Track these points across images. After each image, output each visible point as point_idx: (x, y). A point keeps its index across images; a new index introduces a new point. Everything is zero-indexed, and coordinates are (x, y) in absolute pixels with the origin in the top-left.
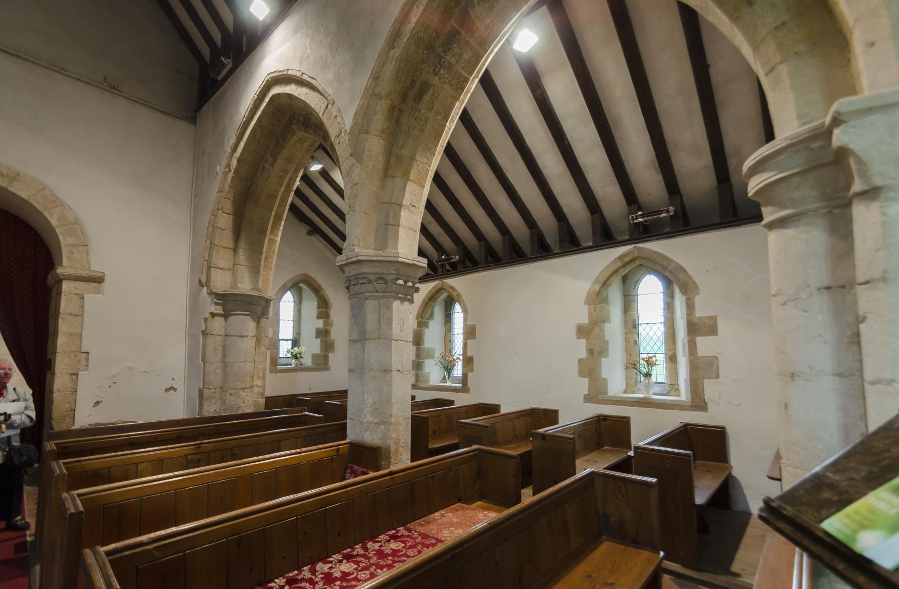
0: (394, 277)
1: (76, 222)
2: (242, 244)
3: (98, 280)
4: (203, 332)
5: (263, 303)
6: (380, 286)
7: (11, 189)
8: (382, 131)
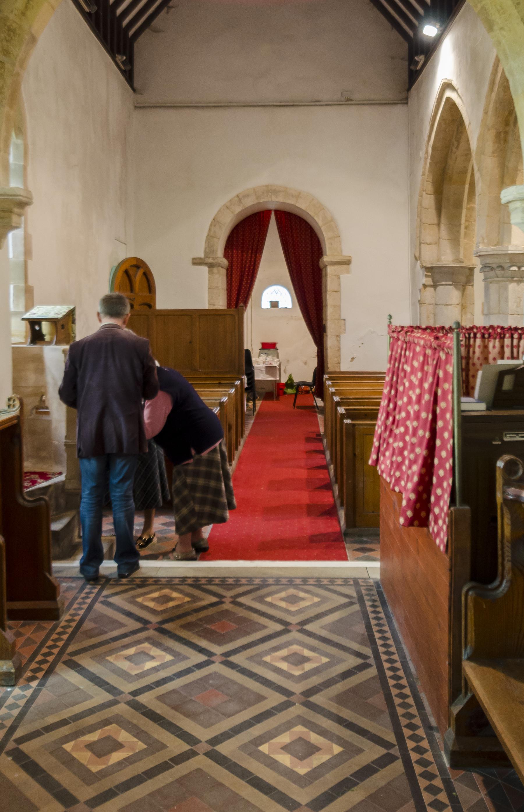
0: (509, 265)
1: (332, 220)
2: (443, 220)
3: (347, 262)
4: (419, 301)
5: (467, 272)
6: (499, 272)
7: (297, 205)
8: (494, 152)
